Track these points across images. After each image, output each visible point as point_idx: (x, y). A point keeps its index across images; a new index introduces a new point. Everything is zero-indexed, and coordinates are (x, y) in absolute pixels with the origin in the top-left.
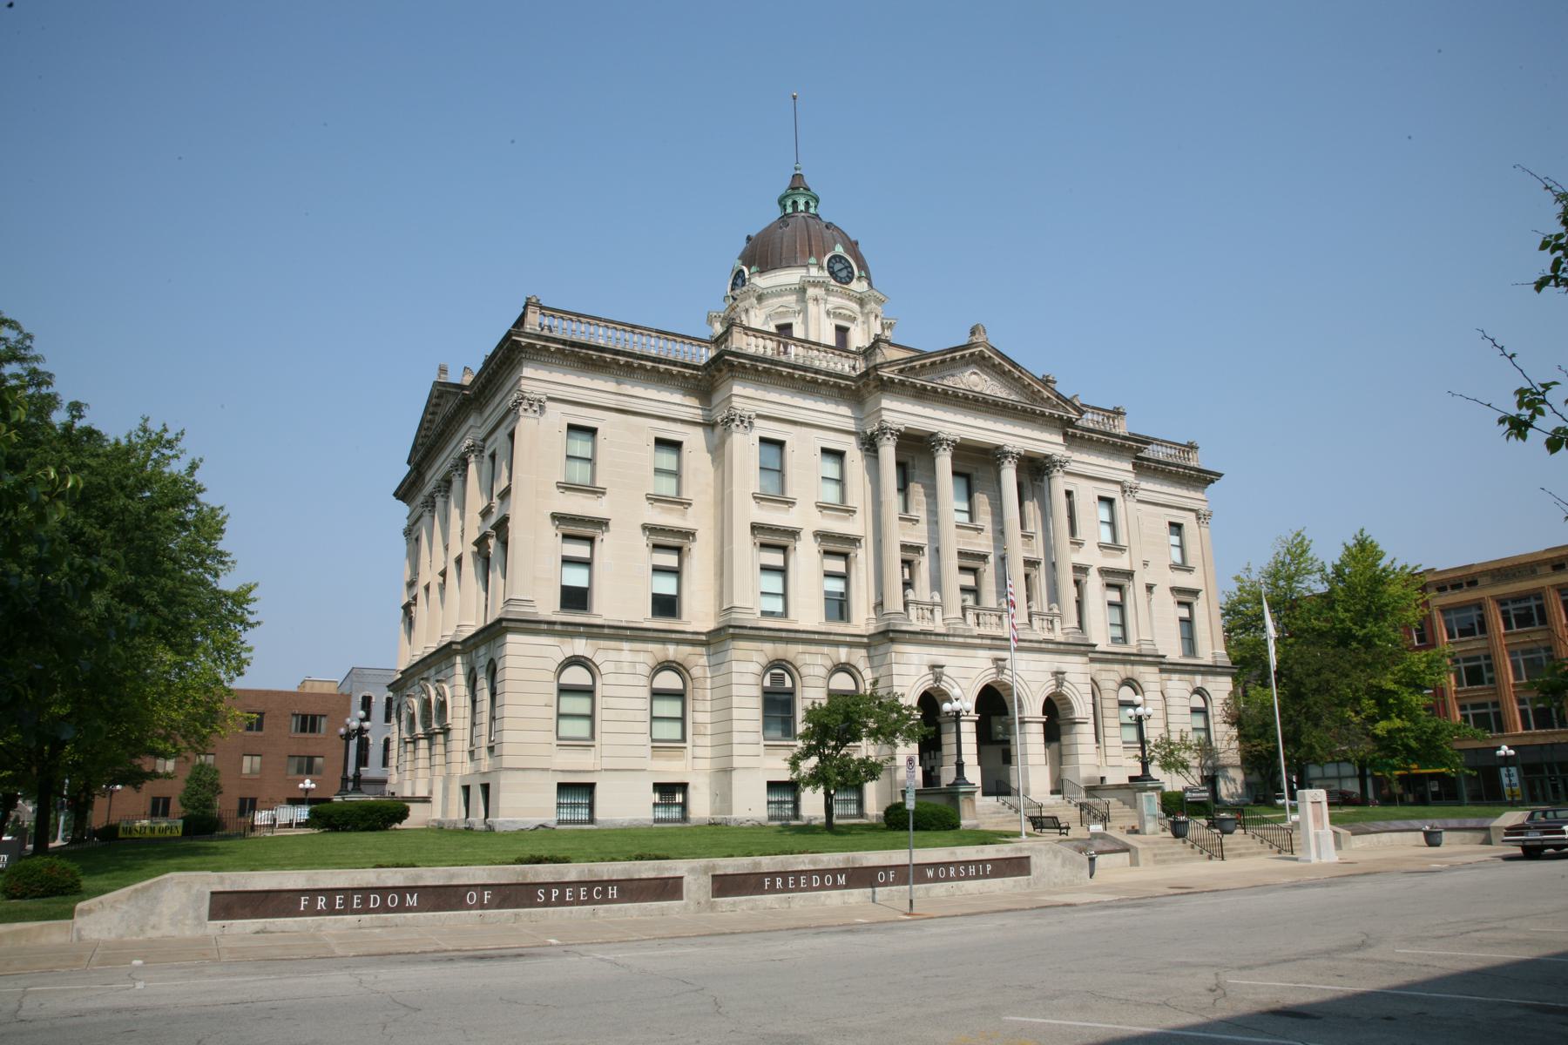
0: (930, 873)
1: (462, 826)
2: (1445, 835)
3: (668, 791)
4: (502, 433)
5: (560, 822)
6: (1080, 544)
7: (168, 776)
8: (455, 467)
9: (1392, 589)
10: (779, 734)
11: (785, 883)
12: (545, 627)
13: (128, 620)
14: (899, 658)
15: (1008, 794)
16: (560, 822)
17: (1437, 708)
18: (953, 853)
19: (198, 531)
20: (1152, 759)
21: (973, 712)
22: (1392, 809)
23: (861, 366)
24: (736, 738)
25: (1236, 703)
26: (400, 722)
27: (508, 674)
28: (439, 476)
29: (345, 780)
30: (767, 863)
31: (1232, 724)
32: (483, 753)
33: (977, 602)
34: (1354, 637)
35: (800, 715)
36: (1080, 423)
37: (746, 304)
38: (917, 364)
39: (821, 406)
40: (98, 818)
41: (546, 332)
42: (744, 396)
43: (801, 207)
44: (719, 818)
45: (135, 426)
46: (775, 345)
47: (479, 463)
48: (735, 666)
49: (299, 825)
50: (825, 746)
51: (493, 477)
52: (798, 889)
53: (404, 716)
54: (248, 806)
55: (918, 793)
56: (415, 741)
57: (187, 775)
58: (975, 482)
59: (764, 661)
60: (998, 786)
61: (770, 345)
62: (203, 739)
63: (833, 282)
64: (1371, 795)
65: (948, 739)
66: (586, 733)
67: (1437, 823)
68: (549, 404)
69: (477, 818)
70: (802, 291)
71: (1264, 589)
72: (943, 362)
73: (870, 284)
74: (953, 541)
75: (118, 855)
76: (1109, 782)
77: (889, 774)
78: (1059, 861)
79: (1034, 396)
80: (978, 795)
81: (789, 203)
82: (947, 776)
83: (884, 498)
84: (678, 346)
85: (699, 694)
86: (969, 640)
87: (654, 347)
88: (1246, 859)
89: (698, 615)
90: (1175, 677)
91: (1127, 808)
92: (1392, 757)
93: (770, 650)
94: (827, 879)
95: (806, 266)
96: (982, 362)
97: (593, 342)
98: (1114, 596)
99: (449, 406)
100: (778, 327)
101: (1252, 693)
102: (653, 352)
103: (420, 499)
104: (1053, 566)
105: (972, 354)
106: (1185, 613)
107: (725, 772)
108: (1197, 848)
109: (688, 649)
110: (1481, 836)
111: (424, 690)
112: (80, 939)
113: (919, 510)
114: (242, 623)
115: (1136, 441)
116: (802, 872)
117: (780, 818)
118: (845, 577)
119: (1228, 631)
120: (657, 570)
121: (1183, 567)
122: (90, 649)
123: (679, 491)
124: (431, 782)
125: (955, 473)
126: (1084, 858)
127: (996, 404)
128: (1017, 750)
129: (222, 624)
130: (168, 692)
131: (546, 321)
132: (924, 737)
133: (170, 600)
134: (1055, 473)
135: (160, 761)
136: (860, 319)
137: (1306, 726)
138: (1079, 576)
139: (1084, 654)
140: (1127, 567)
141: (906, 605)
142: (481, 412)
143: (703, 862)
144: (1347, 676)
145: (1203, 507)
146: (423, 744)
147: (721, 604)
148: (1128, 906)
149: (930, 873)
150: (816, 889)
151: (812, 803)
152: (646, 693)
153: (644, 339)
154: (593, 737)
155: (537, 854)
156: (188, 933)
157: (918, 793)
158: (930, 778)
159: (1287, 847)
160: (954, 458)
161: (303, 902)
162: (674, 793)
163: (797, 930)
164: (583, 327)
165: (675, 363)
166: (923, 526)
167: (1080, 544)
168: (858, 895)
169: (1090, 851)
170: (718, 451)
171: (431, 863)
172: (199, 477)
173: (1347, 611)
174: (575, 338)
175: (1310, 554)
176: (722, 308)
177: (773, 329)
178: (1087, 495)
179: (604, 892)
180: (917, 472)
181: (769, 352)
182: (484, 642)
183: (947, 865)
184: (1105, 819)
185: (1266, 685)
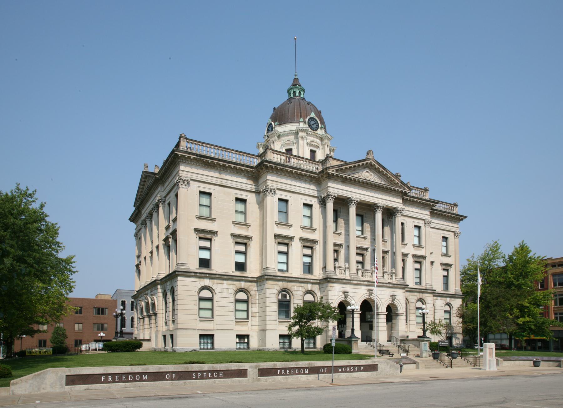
0: (340, 369)
1: (163, 350)
2: (541, 362)
3: (241, 337)
4: (172, 194)
5: (201, 349)
6: (405, 245)
7: (44, 331)
8: (154, 208)
9: (532, 266)
10: (284, 317)
11: (286, 372)
12: (193, 274)
13: (21, 270)
14: (331, 289)
15: (371, 341)
16: (201, 349)
17: (545, 314)
18: (349, 362)
19: (47, 233)
20: (427, 329)
21: (359, 310)
22: (521, 352)
23: (320, 168)
24: (268, 318)
25: (462, 309)
26: (137, 311)
27: (179, 292)
28: (147, 212)
29: (117, 333)
30: (279, 365)
31: (460, 317)
32: (170, 323)
33: (363, 267)
34: (514, 285)
35: (292, 310)
36: (409, 194)
37: (273, 139)
38: (344, 167)
39: (303, 185)
40: (17, 347)
41: (189, 150)
42: (272, 180)
43: (297, 94)
44: (261, 348)
45: (14, 187)
46: (285, 158)
47: (164, 207)
48: (268, 291)
49: (99, 350)
50: (302, 322)
51: (170, 213)
52: (290, 374)
53: (138, 309)
54: (78, 343)
55: (336, 340)
56: (143, 318)
57: (52, 331)
58: (365, 219)
59: (279, 289)
60: (367, 338)
61: (283, 158)
62: (58, 317)
63: (310, 130)
64: (513, 346)
65: (349, 320)
66: (210, 315)
67: (539, 358)
68: (191, 182)
69: (169, 347)
70: (297, 134)
71: (479, 265)
72: (354, 166)
73: (325, 131)
74: (355, 243)
75: (24, 362)
76: (410, 338)
77: (326, 332)
78: (389, 366)
79: (391, 182)
80: (359, 341)
81: (292, 92)
82: (348, 334)
83: (327, 225)
84: (245, 158)
85: (254, 301)
86: (359, 282)
87: (234, 158)
88: (461, 368)
89: (253, 271)
90: (439, 298)
91: (416, 348)
92: (524, 332)
93: (281, 285)
94: (301, 371)
95: (299, 122)
96: (371, 167)
97: (209, 155)
98: (418, 266)
99: (150, 182)
100: (286, 150)
101: (469, 305)
102: (234, 160)
103: (140, 221)
104: (394, 253)
105: (367, 163)
106: (445, 273)
107: (263, 331)
108: (442, 363)
109: (249, 284)
110: (557, 364)
111: (146, 299)
112: (13, 394)
113: (342, 230)
114: (70, 271)
115: (432, 202)
116: (292, 368)
117: (284, 348)
118: (311, 256)
119: (462, 281)
120: (237, 252)
121: (446, 255)
122: (6, 281)
123: (245, 221)
124: (150, 334)
125: (357, 215)
126: (398, 366)
127: (375, 185)
128: (375, 325)
129: (62, 272)
130: (41, 299)
131: (189, 145)
132: (340, 319)
133: (39, 261)
134: (398, 215)
135: (41, 326)
136: (321, 147)
137: (490, 319)
138: (404, 258)
139: (404, 288)
140: (423, 254)
141: (335, 268)
142: (163, 185)
143: (255, 364)
144: (509, 300)
145: (457, 230)
146: (147, 319)
147: (262, 266)
148: (414, 384)
149: (340, 369)
150: (297, 374)
151: (296, 343)
152: (233, 300)
153: (230, 154)
154: (213, 317)
155: (192, 360)
156: (58, 391)
157: (336, 340)
158: (341, 334)
159: (477, 364)
160: (357, 208)
161: (103, 378)
162: (244, 339)
163: (290, 389)
164: (204, 148)
165: (243, 165)
166: (343, 236)
167: (405, 245)
168: (313, 377)
169: (401, 363)
170: (261, 204)
171: (152, 364)
172: (45, 210)
173: (512, 274)
174: (201, 153)
175: (500, 251)
176: (263, 141)
177: (284, 151)
178: (410, 224)
179: (218, 375)
180: (342, 214)
181: (282, 161)
182: (169, 280)
183: (346, 367)
184: (407, 351)
185: (475, 302)
